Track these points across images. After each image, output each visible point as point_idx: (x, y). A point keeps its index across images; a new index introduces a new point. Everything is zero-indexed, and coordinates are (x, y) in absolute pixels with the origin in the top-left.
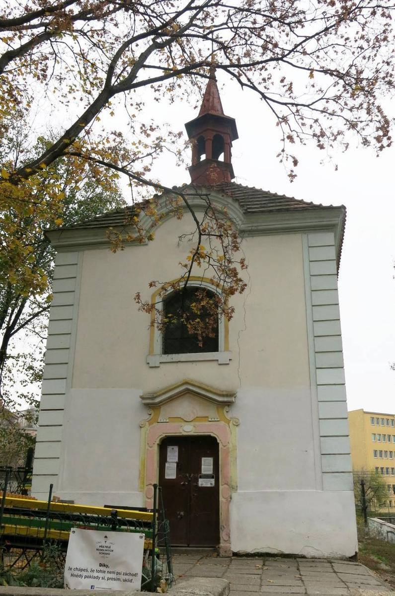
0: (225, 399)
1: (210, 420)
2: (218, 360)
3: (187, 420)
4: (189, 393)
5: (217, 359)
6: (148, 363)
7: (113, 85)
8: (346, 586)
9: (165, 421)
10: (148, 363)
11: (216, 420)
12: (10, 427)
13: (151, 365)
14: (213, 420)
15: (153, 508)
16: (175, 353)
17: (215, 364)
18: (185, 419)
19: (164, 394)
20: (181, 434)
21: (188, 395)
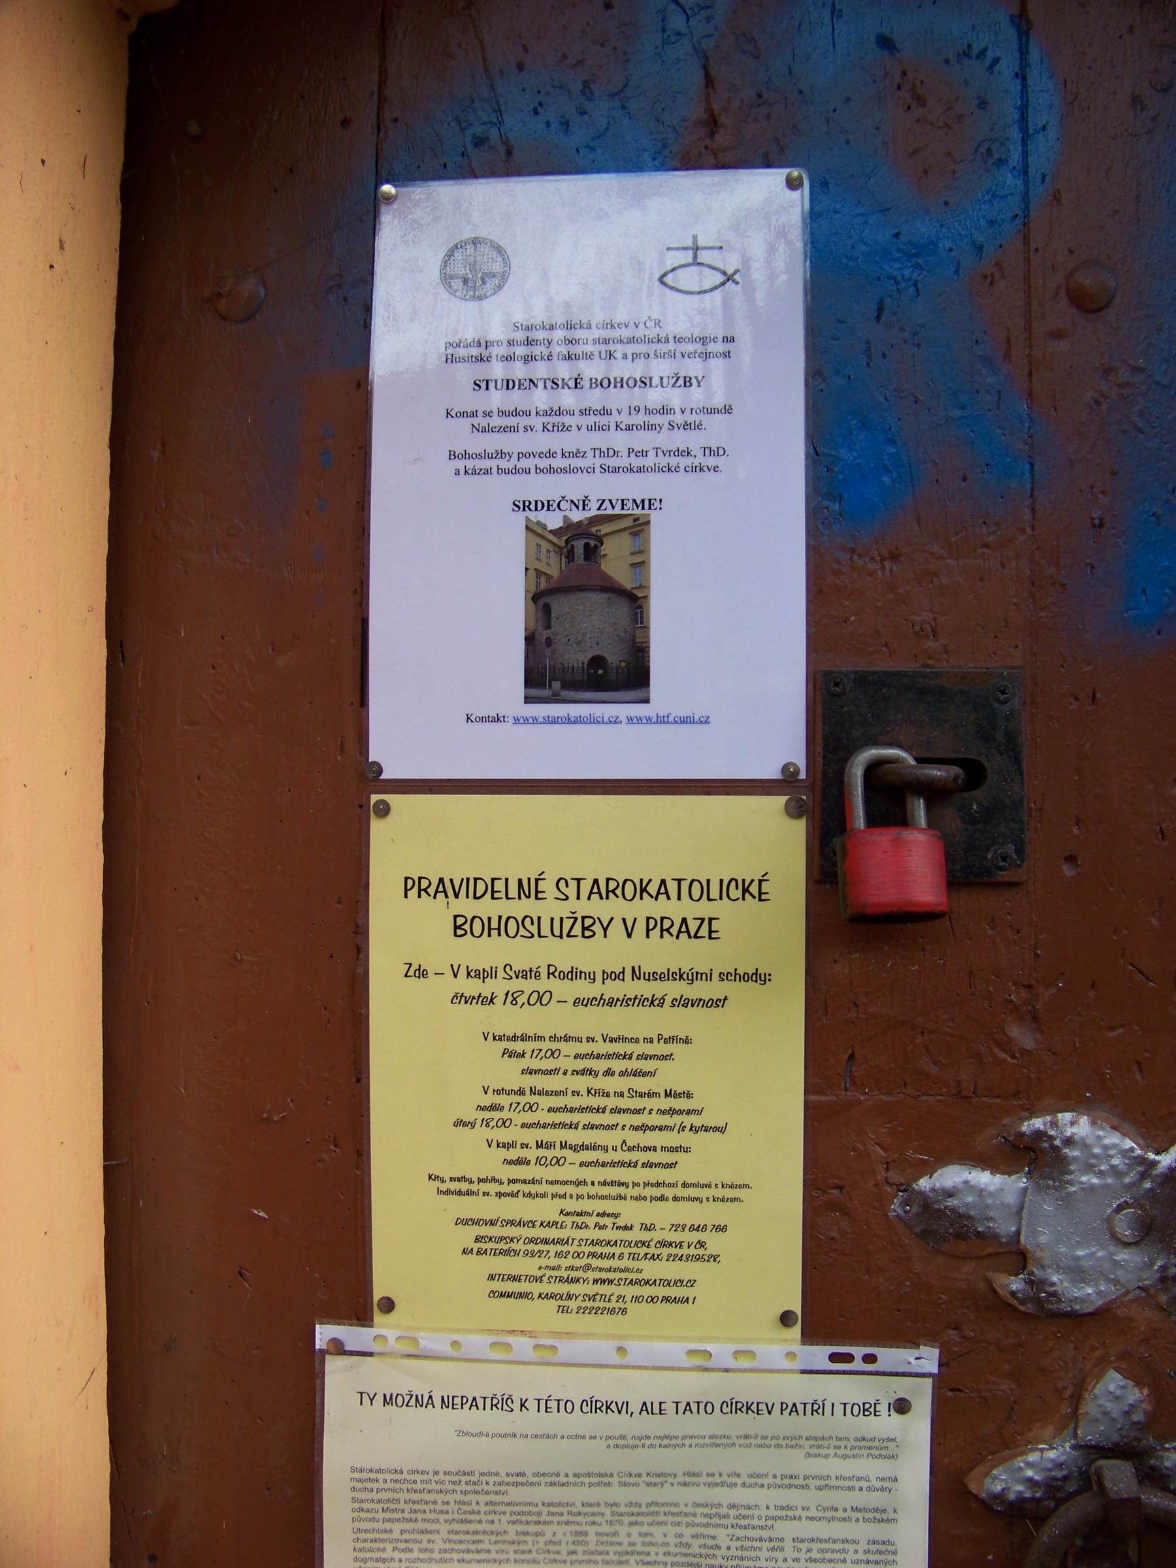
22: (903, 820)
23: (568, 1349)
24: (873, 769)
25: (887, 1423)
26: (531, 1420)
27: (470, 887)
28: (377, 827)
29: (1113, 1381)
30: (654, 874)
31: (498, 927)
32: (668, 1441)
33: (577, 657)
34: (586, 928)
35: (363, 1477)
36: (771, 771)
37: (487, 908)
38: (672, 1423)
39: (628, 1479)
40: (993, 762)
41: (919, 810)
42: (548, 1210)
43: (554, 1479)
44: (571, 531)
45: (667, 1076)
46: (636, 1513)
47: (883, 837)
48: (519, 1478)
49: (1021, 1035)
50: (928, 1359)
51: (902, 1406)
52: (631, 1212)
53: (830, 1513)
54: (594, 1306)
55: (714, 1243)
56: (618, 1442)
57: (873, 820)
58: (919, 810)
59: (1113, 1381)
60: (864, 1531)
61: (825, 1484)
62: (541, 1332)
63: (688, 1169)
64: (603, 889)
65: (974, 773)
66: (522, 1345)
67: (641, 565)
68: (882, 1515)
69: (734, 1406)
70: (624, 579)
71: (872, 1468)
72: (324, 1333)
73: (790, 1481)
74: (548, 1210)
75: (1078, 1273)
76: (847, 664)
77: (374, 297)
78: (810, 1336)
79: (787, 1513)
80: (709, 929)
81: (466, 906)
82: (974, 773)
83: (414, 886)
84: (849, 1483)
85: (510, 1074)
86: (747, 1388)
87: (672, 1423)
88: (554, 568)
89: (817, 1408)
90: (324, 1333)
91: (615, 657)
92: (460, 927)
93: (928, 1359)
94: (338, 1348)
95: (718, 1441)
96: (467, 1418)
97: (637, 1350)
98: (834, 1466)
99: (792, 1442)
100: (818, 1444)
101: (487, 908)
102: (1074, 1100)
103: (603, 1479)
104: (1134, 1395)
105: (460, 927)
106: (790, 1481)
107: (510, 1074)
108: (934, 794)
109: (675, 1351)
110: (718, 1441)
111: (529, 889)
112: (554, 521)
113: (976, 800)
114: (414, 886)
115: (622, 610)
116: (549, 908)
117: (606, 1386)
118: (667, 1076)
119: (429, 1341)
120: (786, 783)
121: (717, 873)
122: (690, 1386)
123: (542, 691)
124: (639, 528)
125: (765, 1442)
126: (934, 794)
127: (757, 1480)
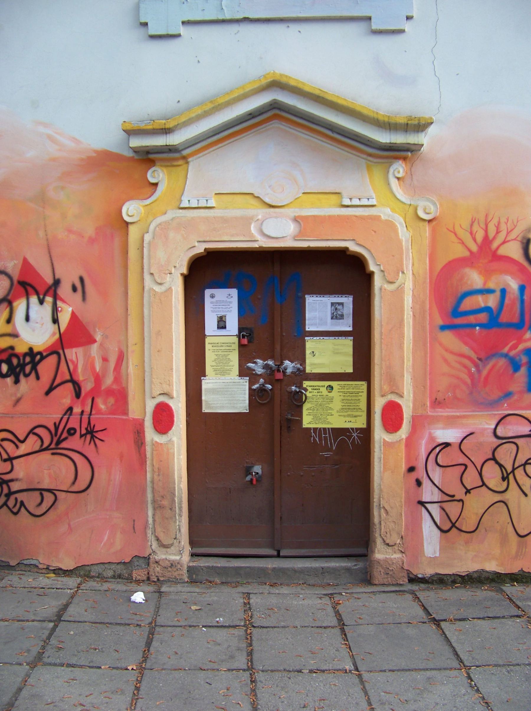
0: (399, 139)
1: (347, 202)
2: (370, 18)
3: (273, 204)
4: (276, 117)
5: (368, 15)
6: (145, 25)
7: (144, 600)
8: (515, 611)
9: (203, 204)
10: (145, 24)
11: (365, 202)
12: (463, 699)
13: (153, 30)
14: (356, 202)
15: (308, 370)
16: (144, 429)
17: (360, 27)
18: (267, 200)
19: (199, 118)
20: (256, 245)
21: (276, 124)
22: (245, 338)
23: (221, 378)
24: (242, 334)
25: (245, 383)
26: (218, 384)
27: (213, 343)
28: (206, 339)
29: (262, 379)
30: (227, 342)
31: (215, 346)
32: (229, 385)
33: (221, 326)
34: (222, 346)
35: (205, 389)
36: (235, 334)
37: (214, 345)
38: (229, 384)
39: (226, 388)
40: (252, 334)
41: (246, 337)
42: (219, 368)
43: (220, 389)
44: (220, 317)
45: (228, 357)
46: (226, 391)
47: (243, 339)
48: (217, 389)
49: (254, 354)
50: (248, 378)
51: (246, 382)
52: (226, 368)
53: (241, 391)
54: (223, 375)
55: (232, 370)
56: (225, 385)
57: (242, 338)
58: (246, 337)
59: (262, 379)
60: (244, 392)
61: (241, 388)
62: (28, 676)
63: (230, 364)
64: (223, 343)
65: (250, 335)
66: (218, 378)
67: (226, 319)
68: (245, 391)
69: (234, 382)
70: (224, 320)
71: (244, 387)
72: (202, 378)
73: (238, 388)
74: (219, 368)
75: (259, 371)
76: (241, 326)
77: (273, 558)
78: (239, 376)
79: (238, 391)
80: (231, 346)
81: (213, 345)
82: (250, 335)
83: (209, 343)
84: (242, 388)
85: (216, 357)
86: (234, 381)
87: (229, 384)
88: (219, 319)
89: (240, 382)
90: (202, 378)
91: (224, 326)
92: (213, 346)
93: (248, 378)
94: (203, 379)
95: (233, 385)
96: (213, 384)
97: (226, 378)
98: (241, 387)
99: (238, 385)
100: (240, 385)
101: (214, 345)
102: (258, 359)
103: (224, 388)
104: (263, 380)
105: (213, 346)
106: (238, 388)
107: (216, 357)
108: (247, 336)
109: (229, 378)
110: (233, 385)
111: (218, 343)
112: (219, 316)
113: (250, 336)
114: (209, 343)
115: (224, 323)
116: (219, 345)
117: (224, 381)
118: (228, 357)
119: (210, 378)
120: (236, 335)
121: (231, 342)
122: (230, 381)
123: (207, 247)
124: (225, 316)
125: (236, 385)
126: (247, 336)
127: (235, 388)
